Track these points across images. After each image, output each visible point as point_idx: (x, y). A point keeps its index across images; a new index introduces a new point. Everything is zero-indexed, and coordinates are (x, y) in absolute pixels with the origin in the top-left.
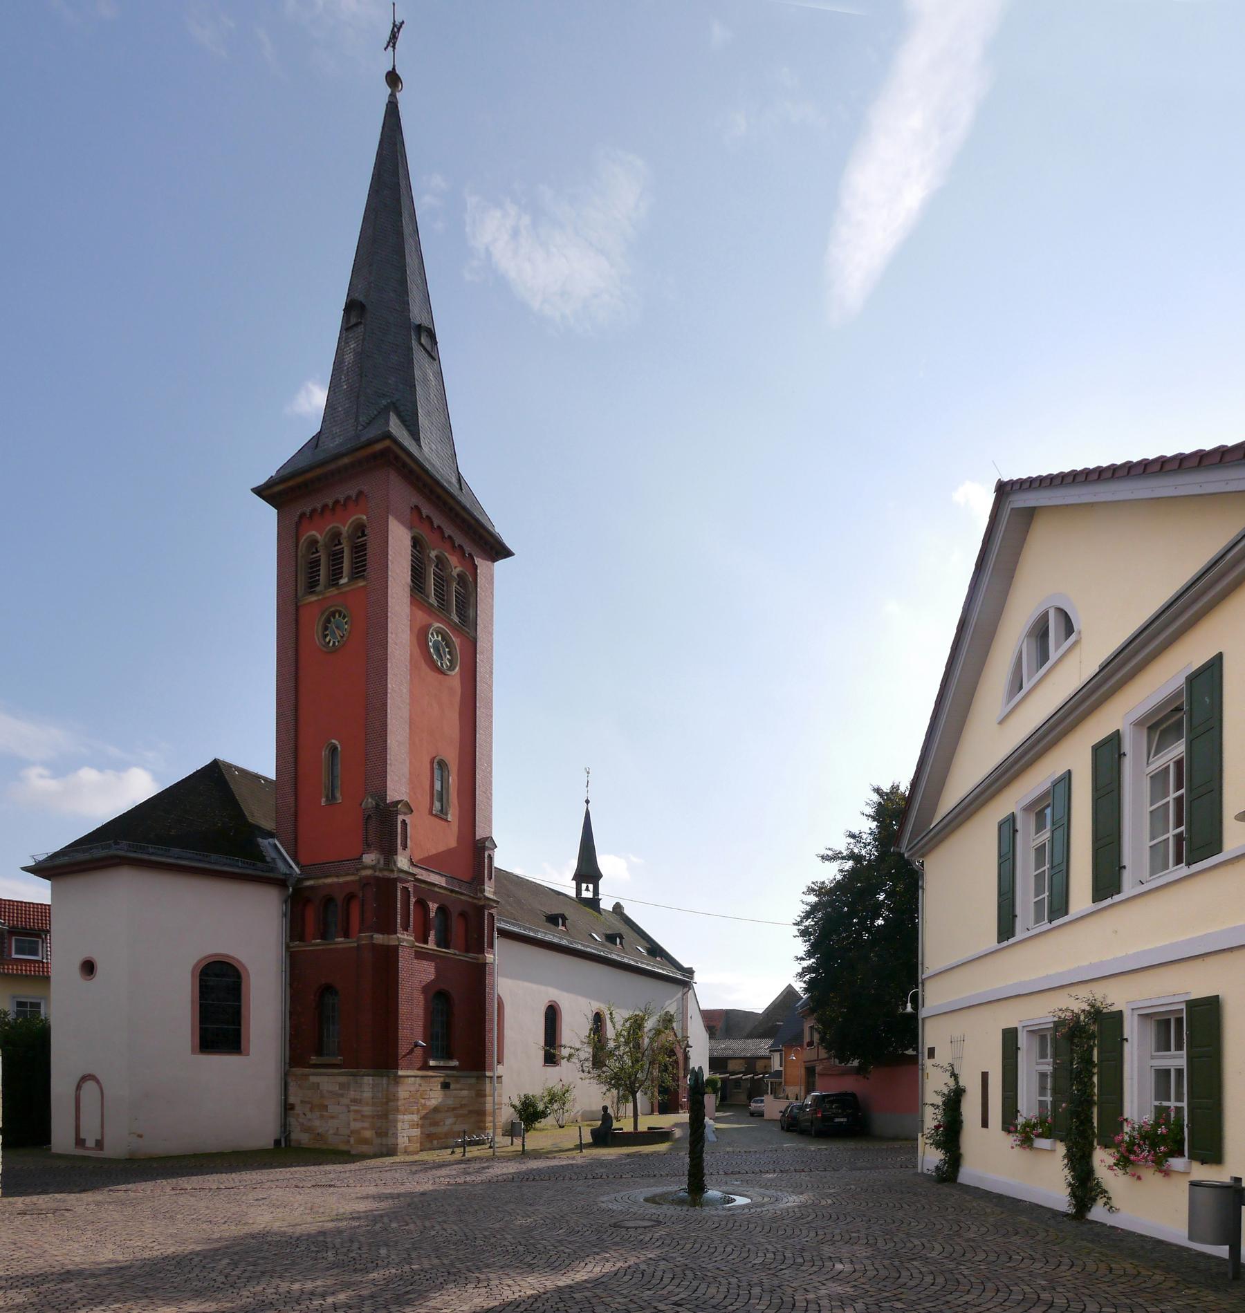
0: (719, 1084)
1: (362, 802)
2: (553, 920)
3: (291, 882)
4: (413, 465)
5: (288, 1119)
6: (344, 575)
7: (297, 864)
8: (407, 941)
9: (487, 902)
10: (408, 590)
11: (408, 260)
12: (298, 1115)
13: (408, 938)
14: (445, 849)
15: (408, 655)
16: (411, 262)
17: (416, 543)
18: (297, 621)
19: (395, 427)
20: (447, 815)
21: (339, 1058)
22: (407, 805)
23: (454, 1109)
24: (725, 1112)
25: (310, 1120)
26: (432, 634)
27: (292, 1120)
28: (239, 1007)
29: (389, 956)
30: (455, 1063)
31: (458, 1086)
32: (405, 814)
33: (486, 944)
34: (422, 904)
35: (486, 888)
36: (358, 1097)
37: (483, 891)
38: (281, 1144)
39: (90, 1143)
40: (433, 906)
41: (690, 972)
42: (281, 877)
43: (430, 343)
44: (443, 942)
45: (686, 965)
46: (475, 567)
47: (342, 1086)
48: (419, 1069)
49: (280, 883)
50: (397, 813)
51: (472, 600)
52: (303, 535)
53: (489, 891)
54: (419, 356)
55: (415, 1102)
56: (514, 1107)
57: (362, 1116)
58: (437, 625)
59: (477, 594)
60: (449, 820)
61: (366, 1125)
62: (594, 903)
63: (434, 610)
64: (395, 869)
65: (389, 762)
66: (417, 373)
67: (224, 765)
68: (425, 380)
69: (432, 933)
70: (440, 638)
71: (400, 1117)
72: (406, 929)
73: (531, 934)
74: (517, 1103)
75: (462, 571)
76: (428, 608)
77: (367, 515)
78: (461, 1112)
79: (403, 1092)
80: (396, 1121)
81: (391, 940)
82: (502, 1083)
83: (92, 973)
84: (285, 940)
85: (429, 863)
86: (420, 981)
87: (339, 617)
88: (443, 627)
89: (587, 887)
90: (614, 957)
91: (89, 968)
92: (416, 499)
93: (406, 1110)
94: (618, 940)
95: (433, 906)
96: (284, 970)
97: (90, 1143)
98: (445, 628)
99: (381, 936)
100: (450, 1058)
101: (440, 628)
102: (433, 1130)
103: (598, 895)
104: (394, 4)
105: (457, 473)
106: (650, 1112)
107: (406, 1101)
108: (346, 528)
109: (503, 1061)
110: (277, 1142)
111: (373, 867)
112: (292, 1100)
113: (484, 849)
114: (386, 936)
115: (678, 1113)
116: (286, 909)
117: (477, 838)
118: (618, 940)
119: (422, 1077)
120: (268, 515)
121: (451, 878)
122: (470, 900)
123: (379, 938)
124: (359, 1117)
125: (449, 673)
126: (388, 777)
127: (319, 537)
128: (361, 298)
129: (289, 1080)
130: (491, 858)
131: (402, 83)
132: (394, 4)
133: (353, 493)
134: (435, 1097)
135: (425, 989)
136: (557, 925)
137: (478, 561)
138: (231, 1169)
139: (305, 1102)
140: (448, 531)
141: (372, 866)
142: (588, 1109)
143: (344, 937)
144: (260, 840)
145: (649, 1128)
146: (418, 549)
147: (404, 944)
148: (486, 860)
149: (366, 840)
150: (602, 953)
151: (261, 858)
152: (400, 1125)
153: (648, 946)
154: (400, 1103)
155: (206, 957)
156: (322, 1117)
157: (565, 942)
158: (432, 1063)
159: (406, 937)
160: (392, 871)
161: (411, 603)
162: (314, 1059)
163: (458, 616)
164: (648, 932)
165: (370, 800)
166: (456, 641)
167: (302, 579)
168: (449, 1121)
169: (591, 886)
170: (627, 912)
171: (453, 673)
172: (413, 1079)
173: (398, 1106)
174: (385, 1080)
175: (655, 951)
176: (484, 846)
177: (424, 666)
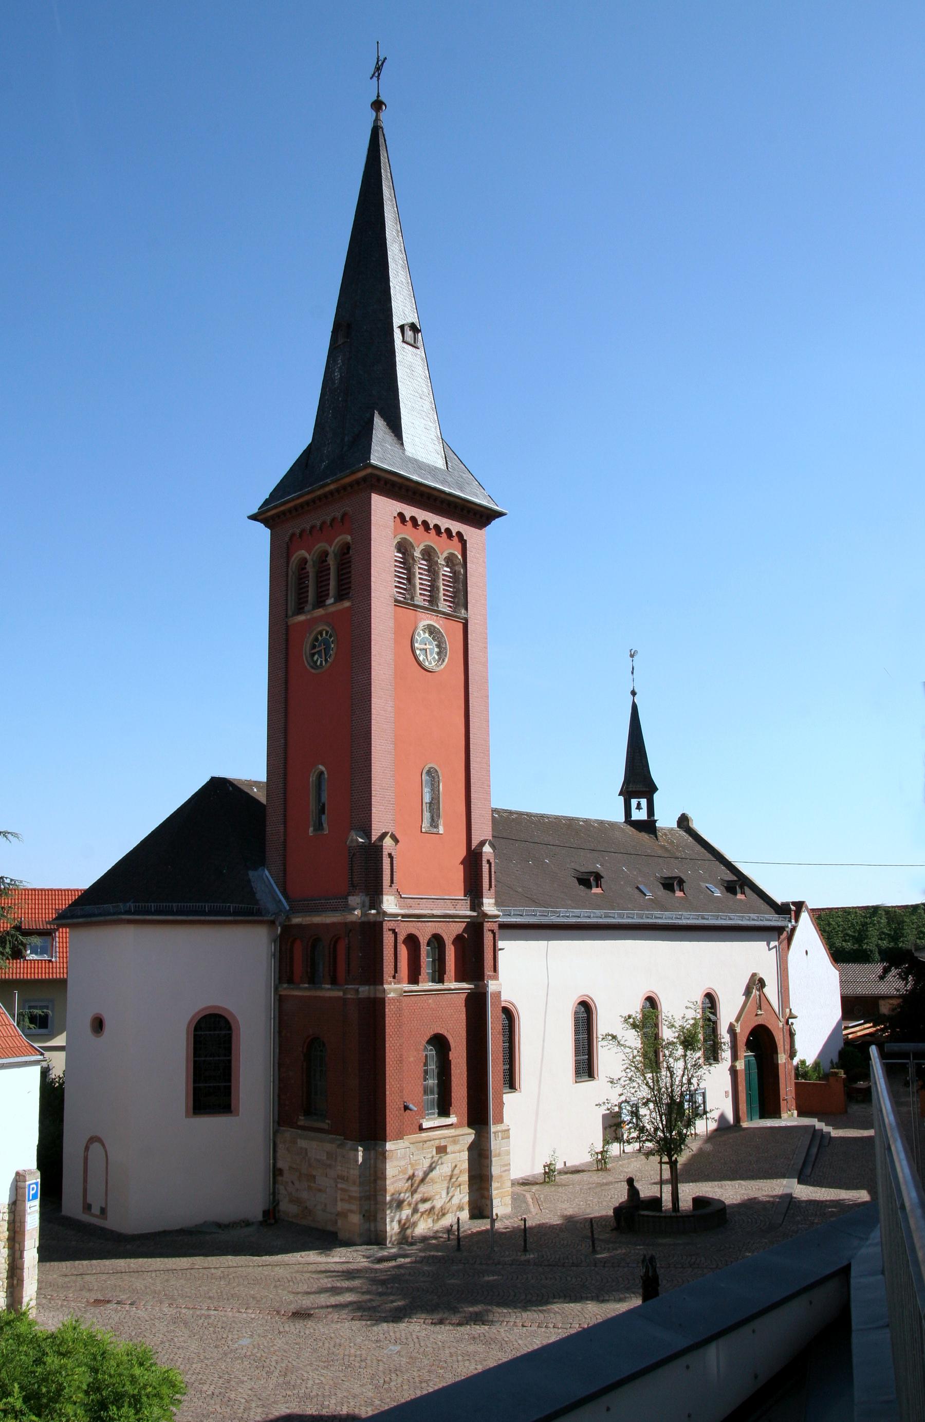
5: (277, 1186)
6: (331, 595)
7: (287, 897)
8: (395, 990)
18: (287, 640)
25: (297, 1190)
27: (281, 1188)
28: (230, 1061)
39: (96, 1210)
47: (330, 1155)
52: (293, 555)
62: (648, 826)
77: (351, 535)
82: (509, 1138)
83: (102, 1030)
84: (274, 981)
89: (639, 804)
91: (98, 1025)
96: (272, 1017)
97: (96, 1210)
103: (653, 815)
108: (332, 548)
110: (266, 1213)
112: (280, 1164)
114: (372, 987)
116: (275, 949)
120: (263, 534)
127: (307, 555)
133: (338, 515)
143: (332, 984)
149: (352, 884)
156: (310, 1188)
162: (302, 1121)
167: (292, 598)
169: (644, 802)
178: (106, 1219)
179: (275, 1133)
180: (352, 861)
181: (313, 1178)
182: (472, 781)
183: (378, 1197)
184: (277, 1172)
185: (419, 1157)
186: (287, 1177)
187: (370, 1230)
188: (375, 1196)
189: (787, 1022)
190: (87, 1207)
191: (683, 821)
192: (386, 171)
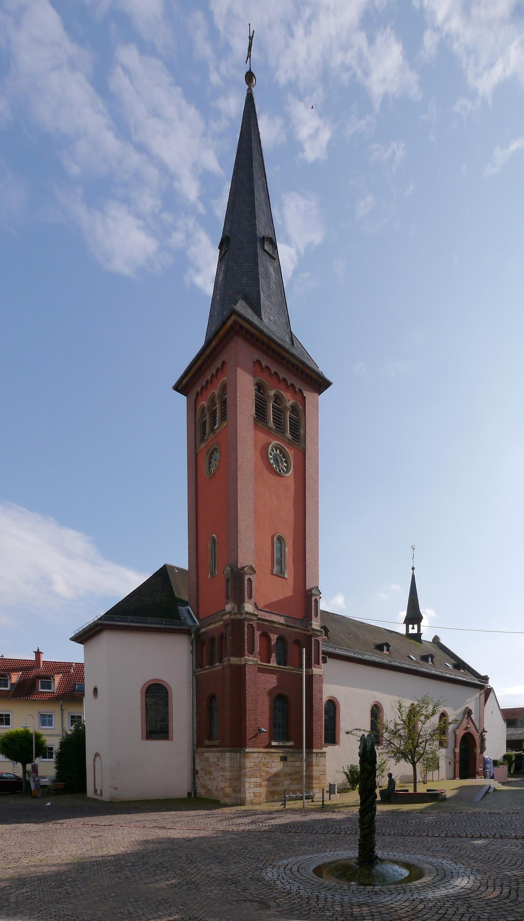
0: (514, 758)
1: (225, 569)
2: (380, 647)
3: (193, 630)
4: (253, 330)
7: (198, 619)
8: (252, 661)
9: (314, 632)
10: (252, 420)
11: (257, 195)
12: (200, 777)
13: (253, 659)
14: (284, 597)
15: (253, 466)
16: (259, 196)
17: (260, 387)
19: (241, 307)
20: (284, 573)
21: (218, 741)
22: (251, 568)
23: (290, 775)
24: (517, 777)
26: (272, 450)
29: (240, 671)
30: (291, 743)
31: (294, 759)
32: (251, 574)
33: (313, 662)
34: (265, 636)
35: (313, 622)
36: (223, 766)
37: (311, 624)
38: (191, 795)
39: (99, 792)
40: (274, 637)
41: (486, 679)
42: (187, 628)
43: (271, 249)
44: (282, 661)
45: (483, 674)
46: (304, 398)
47: (218, 758)
48: (264, 748)
49: (187, 632)
50: (245, 574)
51: (302, 422)
53: (316, 624)
54: (262, 258)
55: (258, 770)
56: (345, 773)
57: (225, 779)
58: (274, 442)
59: (305, 417)
60: (285, 577)
61: (227, 784)
62: (417, 637)
63: (273, 432)
64: (243, 612)
65: (239, 540)
66: (261, 270)
67: (169, 567)
68: (267, 276)
69: (274, 655)
70: (278, 452)
71: (247, 780)
72: (252, 652)
73: (359, 656)
74: (346, 770)
75: (293, 403)
76: (268, 431)
78: (296, 777)
79: (249, 763)
80: (245, 782)
81: (241, 661)
85: (272, 608)
86: (265, 688)
87: (216, 453)
88: (279, 443)
89: (413, 626)
90: (424, 670)
92: (257, 355)
93: (251, 775)
94: (430, 659)
95: (274, 637)
98: (281, 444)
99: (236, 659)
100: (288, 740)
101: (278, 444)
102: (275, 788)
104: (249, 25)
105: (290, 334)
106: (453, 778)
107: (251, 769)
109: (339, 742)
110: (189, 794)
111: (229, 613)
113: (312, 595)
114: (239, 658)
115: (476, 778)
117: (307, 588)
118: (430, 659)
119: (263, 753)
120: (182, 400)
121: (287, 617)
122: (302, 632)
123: (234, 660)
124: (224, 779)
125: (285, 475)
126: (239, 550)
128: (228, 235)
129: (196, 755)
130: (317, 601)
131: (255, 78)
132: (249, 25)
134: (277, 766)
135: (270, 693)
136: (383, 650)
137: (306, 394)
138: (160, 810)
139: (203, 769)
140: (282, 375)
141: (229, 612)
142: (404, 774)
144: (180, 607)
145: (428, 790)
146: (295, 414)
147: (250, 663)
148: (313, 604)
150: (414, 668)
151: (178, 618)
152: (247, 785)
153: (455, 662)
154: (247, 770)
155: (147, 682)
157: (386, 661)
158: (274, 743)
159: (251, 658)
160: (242, 614)
161: (255, 429)
162: (207, 742)
163: (291, 435)
164: (457, 655)
165: (228, 568)
166: (290, 453)
168: (287, 783)
170: (442, 641)
171: (288, 475)
172: (257, 754)
173: (245, 772)
174: (238, 755)
175: (460, 665)
176: (312, 594)
177: (266, 473)
178: (102, 796)
179: (194, 752)
180: (227, 584)
181: (211, 773)
182: (307, 551)
183: (242, 779)
184: (195, 773)
185: (269, 761)
186: (200, 774)
187: (237, 797)
188: (240, 778)
189: (482, 733)
190: (95, 791)
191: (436, 639)
192: (256, 151)
